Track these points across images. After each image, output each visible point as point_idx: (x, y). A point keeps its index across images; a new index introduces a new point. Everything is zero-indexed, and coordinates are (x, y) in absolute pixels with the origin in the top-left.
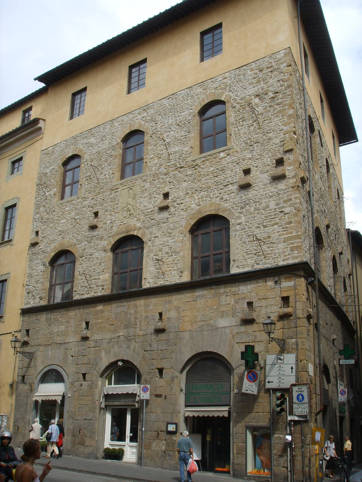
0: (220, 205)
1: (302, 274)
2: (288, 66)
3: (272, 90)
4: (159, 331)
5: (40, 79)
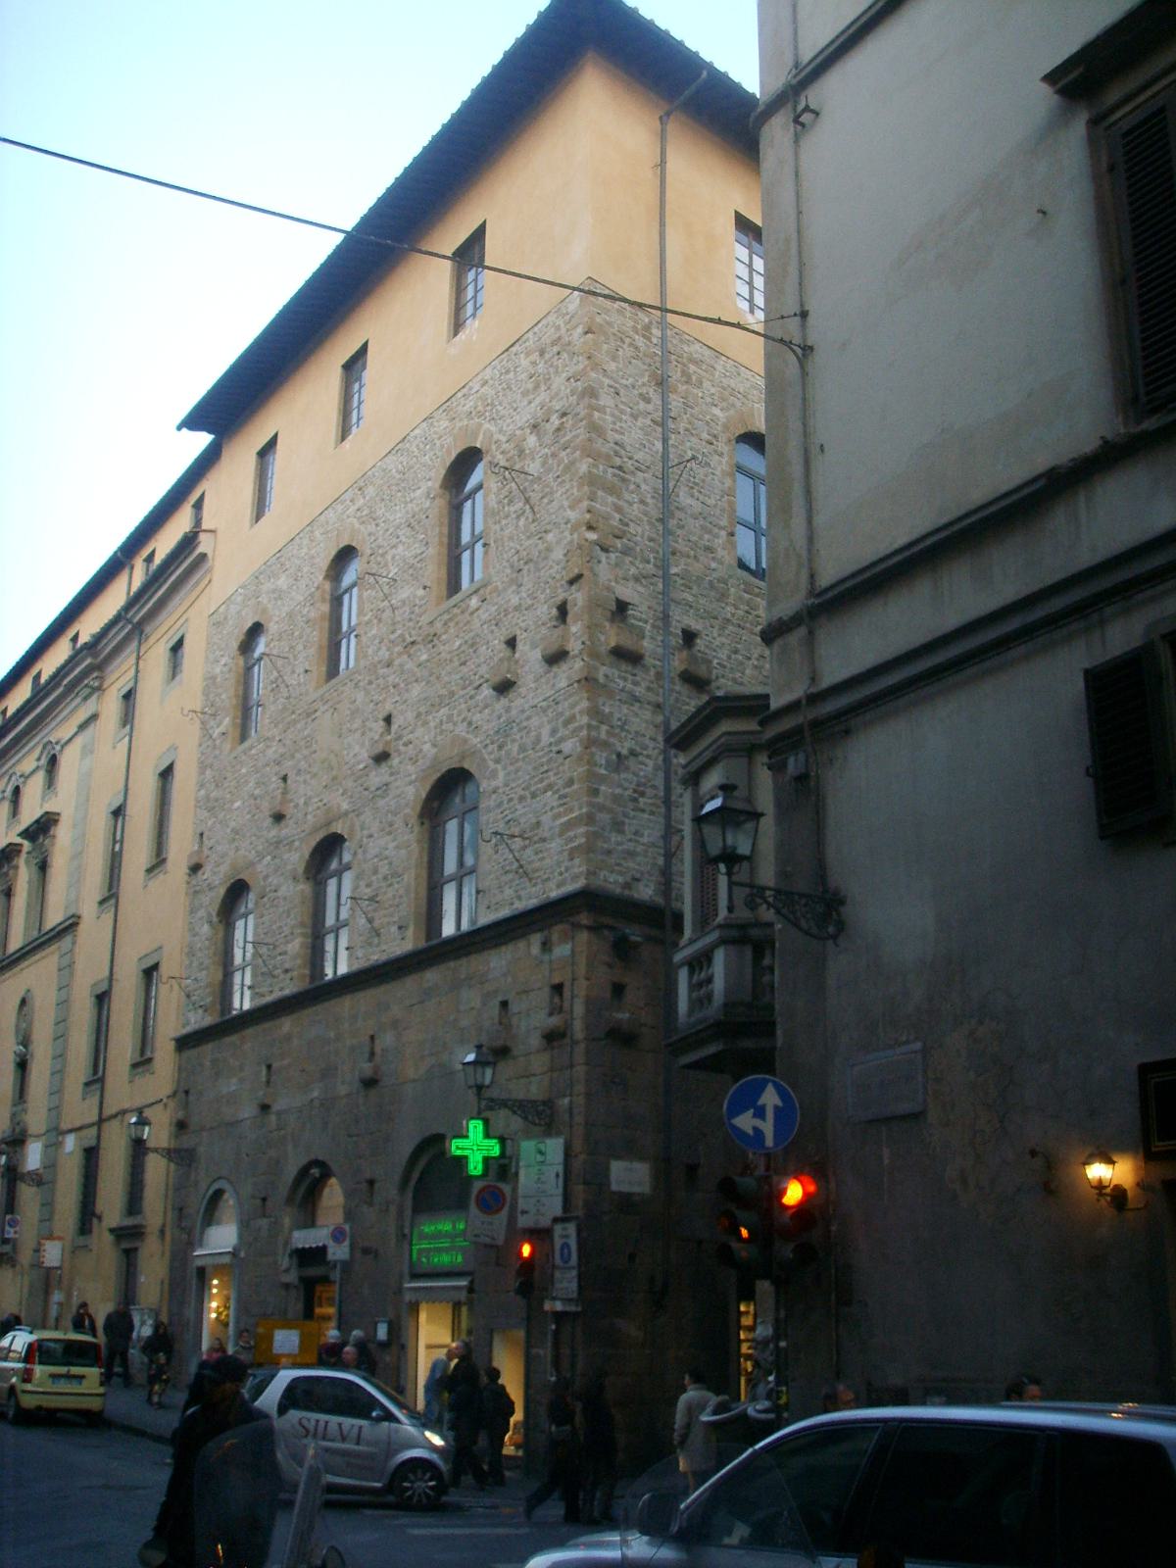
0: (466, 741)
1: (585, 922)
2: (586, 333)
3: (557, 408)
4: (370, 1083)
5: (195, 420)
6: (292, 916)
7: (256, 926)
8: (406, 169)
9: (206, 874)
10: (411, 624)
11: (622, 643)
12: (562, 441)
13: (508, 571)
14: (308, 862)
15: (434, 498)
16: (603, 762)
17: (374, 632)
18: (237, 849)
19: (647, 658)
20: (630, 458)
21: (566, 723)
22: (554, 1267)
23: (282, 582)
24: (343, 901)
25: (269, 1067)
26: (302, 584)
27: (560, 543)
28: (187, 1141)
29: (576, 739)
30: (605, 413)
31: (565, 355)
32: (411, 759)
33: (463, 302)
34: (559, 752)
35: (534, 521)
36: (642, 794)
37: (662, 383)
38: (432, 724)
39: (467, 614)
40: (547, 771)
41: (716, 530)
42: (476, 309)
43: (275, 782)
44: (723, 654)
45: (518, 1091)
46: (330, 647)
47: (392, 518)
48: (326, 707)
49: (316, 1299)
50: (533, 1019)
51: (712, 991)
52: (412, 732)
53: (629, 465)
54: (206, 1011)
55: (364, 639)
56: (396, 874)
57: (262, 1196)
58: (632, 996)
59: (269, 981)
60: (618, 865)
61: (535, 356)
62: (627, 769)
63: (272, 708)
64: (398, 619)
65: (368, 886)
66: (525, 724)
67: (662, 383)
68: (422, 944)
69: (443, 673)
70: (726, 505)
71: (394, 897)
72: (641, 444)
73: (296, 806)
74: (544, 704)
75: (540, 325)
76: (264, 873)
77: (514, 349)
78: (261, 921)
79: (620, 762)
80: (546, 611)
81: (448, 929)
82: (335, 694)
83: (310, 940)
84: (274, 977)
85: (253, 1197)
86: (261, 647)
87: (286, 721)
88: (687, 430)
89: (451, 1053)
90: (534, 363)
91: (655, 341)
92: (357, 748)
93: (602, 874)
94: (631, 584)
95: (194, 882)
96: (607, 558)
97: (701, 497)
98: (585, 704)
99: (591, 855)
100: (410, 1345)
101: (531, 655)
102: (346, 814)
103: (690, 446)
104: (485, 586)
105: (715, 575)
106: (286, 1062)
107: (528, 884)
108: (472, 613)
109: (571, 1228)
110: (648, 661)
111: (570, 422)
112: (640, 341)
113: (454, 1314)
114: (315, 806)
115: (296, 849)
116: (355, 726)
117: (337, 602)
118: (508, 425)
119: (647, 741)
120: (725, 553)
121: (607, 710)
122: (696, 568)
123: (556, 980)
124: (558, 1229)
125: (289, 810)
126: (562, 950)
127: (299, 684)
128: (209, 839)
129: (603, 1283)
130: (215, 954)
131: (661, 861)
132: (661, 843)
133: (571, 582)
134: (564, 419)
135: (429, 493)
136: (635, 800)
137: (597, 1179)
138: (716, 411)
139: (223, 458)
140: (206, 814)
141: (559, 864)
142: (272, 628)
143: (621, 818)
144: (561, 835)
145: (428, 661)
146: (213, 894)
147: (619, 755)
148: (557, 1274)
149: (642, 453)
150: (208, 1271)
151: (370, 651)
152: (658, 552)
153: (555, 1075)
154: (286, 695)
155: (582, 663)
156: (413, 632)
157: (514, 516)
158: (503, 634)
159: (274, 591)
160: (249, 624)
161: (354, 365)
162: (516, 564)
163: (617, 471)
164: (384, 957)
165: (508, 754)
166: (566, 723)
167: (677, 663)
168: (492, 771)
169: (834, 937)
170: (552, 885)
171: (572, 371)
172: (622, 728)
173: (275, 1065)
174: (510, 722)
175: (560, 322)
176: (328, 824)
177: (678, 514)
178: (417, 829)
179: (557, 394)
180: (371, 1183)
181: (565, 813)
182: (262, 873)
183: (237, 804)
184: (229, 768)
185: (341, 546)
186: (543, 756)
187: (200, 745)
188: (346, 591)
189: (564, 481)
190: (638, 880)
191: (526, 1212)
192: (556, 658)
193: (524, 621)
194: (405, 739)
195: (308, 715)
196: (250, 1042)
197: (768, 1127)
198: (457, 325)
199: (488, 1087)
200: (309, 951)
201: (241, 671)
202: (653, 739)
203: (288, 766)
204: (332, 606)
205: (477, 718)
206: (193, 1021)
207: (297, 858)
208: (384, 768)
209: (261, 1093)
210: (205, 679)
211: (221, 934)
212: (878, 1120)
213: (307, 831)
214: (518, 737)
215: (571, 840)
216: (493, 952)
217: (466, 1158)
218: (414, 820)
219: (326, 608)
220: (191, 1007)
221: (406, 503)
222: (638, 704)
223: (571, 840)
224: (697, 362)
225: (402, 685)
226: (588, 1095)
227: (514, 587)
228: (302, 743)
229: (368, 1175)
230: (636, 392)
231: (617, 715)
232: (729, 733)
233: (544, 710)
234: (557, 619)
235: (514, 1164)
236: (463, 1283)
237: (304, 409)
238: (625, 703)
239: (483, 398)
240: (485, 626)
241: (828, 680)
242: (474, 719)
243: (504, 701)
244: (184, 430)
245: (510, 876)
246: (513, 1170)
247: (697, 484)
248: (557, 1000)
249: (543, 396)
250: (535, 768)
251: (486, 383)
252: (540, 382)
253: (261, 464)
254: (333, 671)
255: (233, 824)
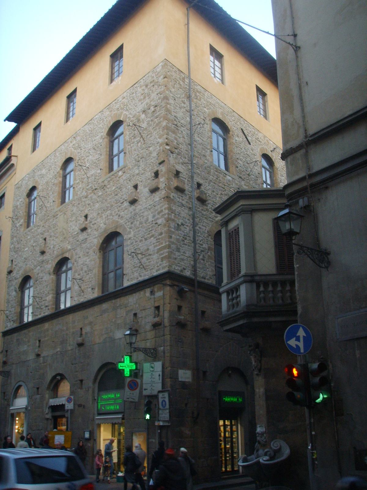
1: (168, 283)
2: (164, 78)
4: (80, 345)
5: (10, 118)
6: (48, 287)
7: (34, 291)
8: (87, 33)
9: (14, 274)
10: (95, 182)
11: (179, 185)
12: (155, 115)
13: (134, 162)
14: (54, 268)
15: (104, 139)
16: (173, 227)
17: (80, 186)
18: (26, 265)
19: (186, 191)
20: (179, 122)
21: (159, 213)
22: (159, 409)
23: (44, 171)
24: (30, 297)
25: (40, 341)
26: (52, 172)
27: (155, 152)
28: (7, 368)
29: (163, 218)
30: (171, 105)
31: (156, 86)
32: (95, 229)
33: (113, 72)
34: (156, 223)
35: (144, 144)
36: (186, 239)
37: (189, 97)
38: (104, 217)
39: (117, 178)
40: (151, 231)
41: (206, 150)
42: (119, 74)
43: (41, 241)
44: (210, 192)
45: (142, 345)
46: (62, 193)
47: (87, 147)
48: (61, 213)
49: (58, 423)
50: (147, 319)
51: (240, 301)
52: (96, 220)
53: (179, 124)
54: (14, 322)
55: (76, 189)
56: (90, 270)
57: (37, 387)
58: (185, 310)
59: (39, 310)
60: (178, 263)
61: (144, 87)
62: (180, 230)
63: (40, 215)
64: (90, 181)
65: (79, 275)
66: (141, 214)
67: (189, 97)
68: (100, 294)
69: (108, 199)
70: (209, 141)
71: (89, 278)
72: (182, 117)
73: (50, 248)
74: (150, 207)
75: (145, 77)
76: (37, 273)
77: (135, 86)
78: (36, 289)
79: (178, 227)
80: (150, 174)
81: (62, 307)
82: (65, 209)
83: (55, 296)
84: (41, 309)
85: (34, 387)
86: (35, 194)
87: (46, 219)
88: (197, 115)
89: (114, 333)
90: (144, 90)
91: (186, 83)
92: (74, 227)
93: (173, 266)
94: (180, 165)
95: (9, 277)
96: (173, 155)
97: (202, 138)
98: (167, 206)
99: (170, 260)
100: (98, 440)
101: (144, 191)
102: (70, 250)
103: (197, 120)
104: (125, 167)
105: (206, 165)
106: (46, 339)
107: (144, 271)
108: (120, 177)
109: (166, 395)
110: (186, 192)
111: (159, 108)
112: (182, 83)
113: (112, 427)
114: (57, 248)
115: (50, 264)
116: (73, 219)
117: (65, 177)
118: (133, 112)
119: (187, 220)
120: (209, 158)
121: (174, 208)
122: (201, 162)
123: (157, 305)
124: (160, 395)
125: (47, 250)
126: (159, 294)
127: (51, 206)
128: (15, 262)
129: (177, 413)
130: (18, 302)
131: (192, 263)
132: (192, 256)
133: (160, 164)
134: (156, 108)
135: (102, 137)
136: (183, 241)
137: (174, 377)
138: (205, 109)
139: (20, 131)
140: (14, 253)
141: (157, 263)
142: (40, 188)
143: (179, 247)
144: (157, 253)
145: (102, 195)
146: (17, 281)
147: (178, 224)
148: (160, 412)
149: (183, 121)
150: (15, 415)
151: (79, 193)
152: (189, 155)
153: (157, 339)
154: (45, 210)
155: (165, 191)
156: (96, 186)
157: (136, 142)
158: (133, 183)
159: (40, 175)
160: (31, 187)
161: (71, 97)
162: (137, 159)
163: (175, 126)
164: (85, 300)
165: (135, 225)
166: (159, 213)
167: (195, 194)
168: (129, 231)
169: (327, 267)
170: (154, 271)
171: (159, 91)
172: (178, 215)
173: (42, 340)
174: (135, 214)
175: (154, 75)
176: (63, 254)
177: (195, 143)
178: (98, 254)
179: (153, 99)
180: (81, 381)
181: (159, 245)
182: (36, 272)
183: (26, 249)
184: (23, 237)
185: (67, 157)
186: (149, 225)
187: (12, 230)
188: (68, 174)
189: (156, 129)
190: (185, 269)
191: (147, 389)
192: (154, 190)
193: (140, 179)
194: (93, 223)
195: (54, 216)
196: (32, 332)
197: (301, 345)
198: (112, 80)
199: (134, 343)
200: (55, 300)
201: (27, 203)
202: (188, 220)
203: (46, 235)
204: (63, 179)
205: (122, 213)
206: (9, 326)
207: (50, 266)
208: (85, 233)
209: (37, 350)
210: (13, 207)
211: (20, 295)
212: (354, 339)
213: (54, 257)
214: (139, 219)
215: (162, 254)
216: (129, 296)
217: (123, 370)
218: (97, 251)
219: (61, 179)
220: (8, 321)
221: (92, 141)
222: (183, 207)
223: (162, 254)
224: (200, 92)
225: (92, 204)
226: (171, 346)
227: (137, 167)
228: (52, 226)
229: (81, 379)
230: (180, 99)
231: (177, 211)
232: (242, 205)
233: (149, 209)
234: (154, 177)
235: (141, 372)
236: (120, 416)
237: (52, 114)
238: (180, 206)
239: (123, 103)
240: (125, 181)
241: (316, 169)
242: (121, 214)
243: (133, 207)
244: (7, 121)
245: (137, 269)
246: (141, 374)
247: (200, 133)
248: (157, 312)
249: (147, 100)
250: (146, 230)
251: (124, 98)
252: (145, 96)
253: (35, 133)
254: (63, 201)
255: (24, 256)
